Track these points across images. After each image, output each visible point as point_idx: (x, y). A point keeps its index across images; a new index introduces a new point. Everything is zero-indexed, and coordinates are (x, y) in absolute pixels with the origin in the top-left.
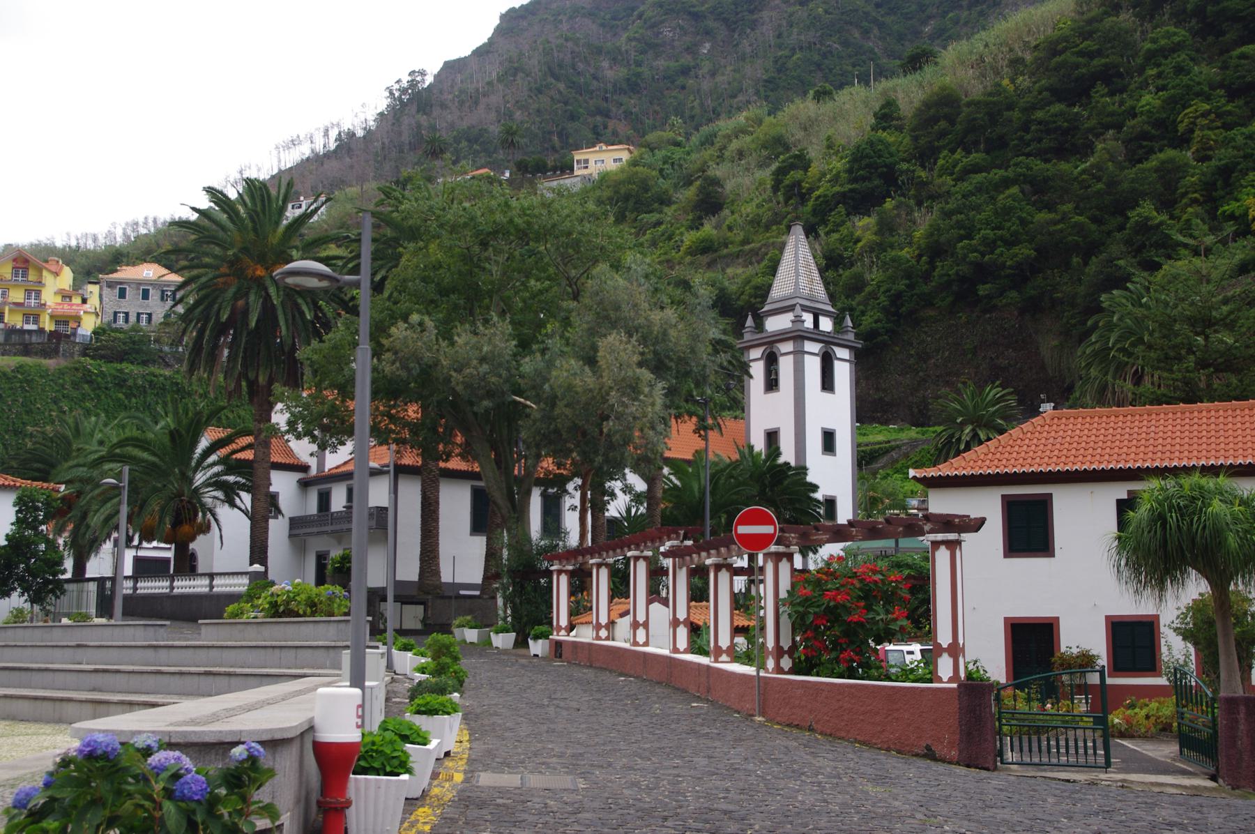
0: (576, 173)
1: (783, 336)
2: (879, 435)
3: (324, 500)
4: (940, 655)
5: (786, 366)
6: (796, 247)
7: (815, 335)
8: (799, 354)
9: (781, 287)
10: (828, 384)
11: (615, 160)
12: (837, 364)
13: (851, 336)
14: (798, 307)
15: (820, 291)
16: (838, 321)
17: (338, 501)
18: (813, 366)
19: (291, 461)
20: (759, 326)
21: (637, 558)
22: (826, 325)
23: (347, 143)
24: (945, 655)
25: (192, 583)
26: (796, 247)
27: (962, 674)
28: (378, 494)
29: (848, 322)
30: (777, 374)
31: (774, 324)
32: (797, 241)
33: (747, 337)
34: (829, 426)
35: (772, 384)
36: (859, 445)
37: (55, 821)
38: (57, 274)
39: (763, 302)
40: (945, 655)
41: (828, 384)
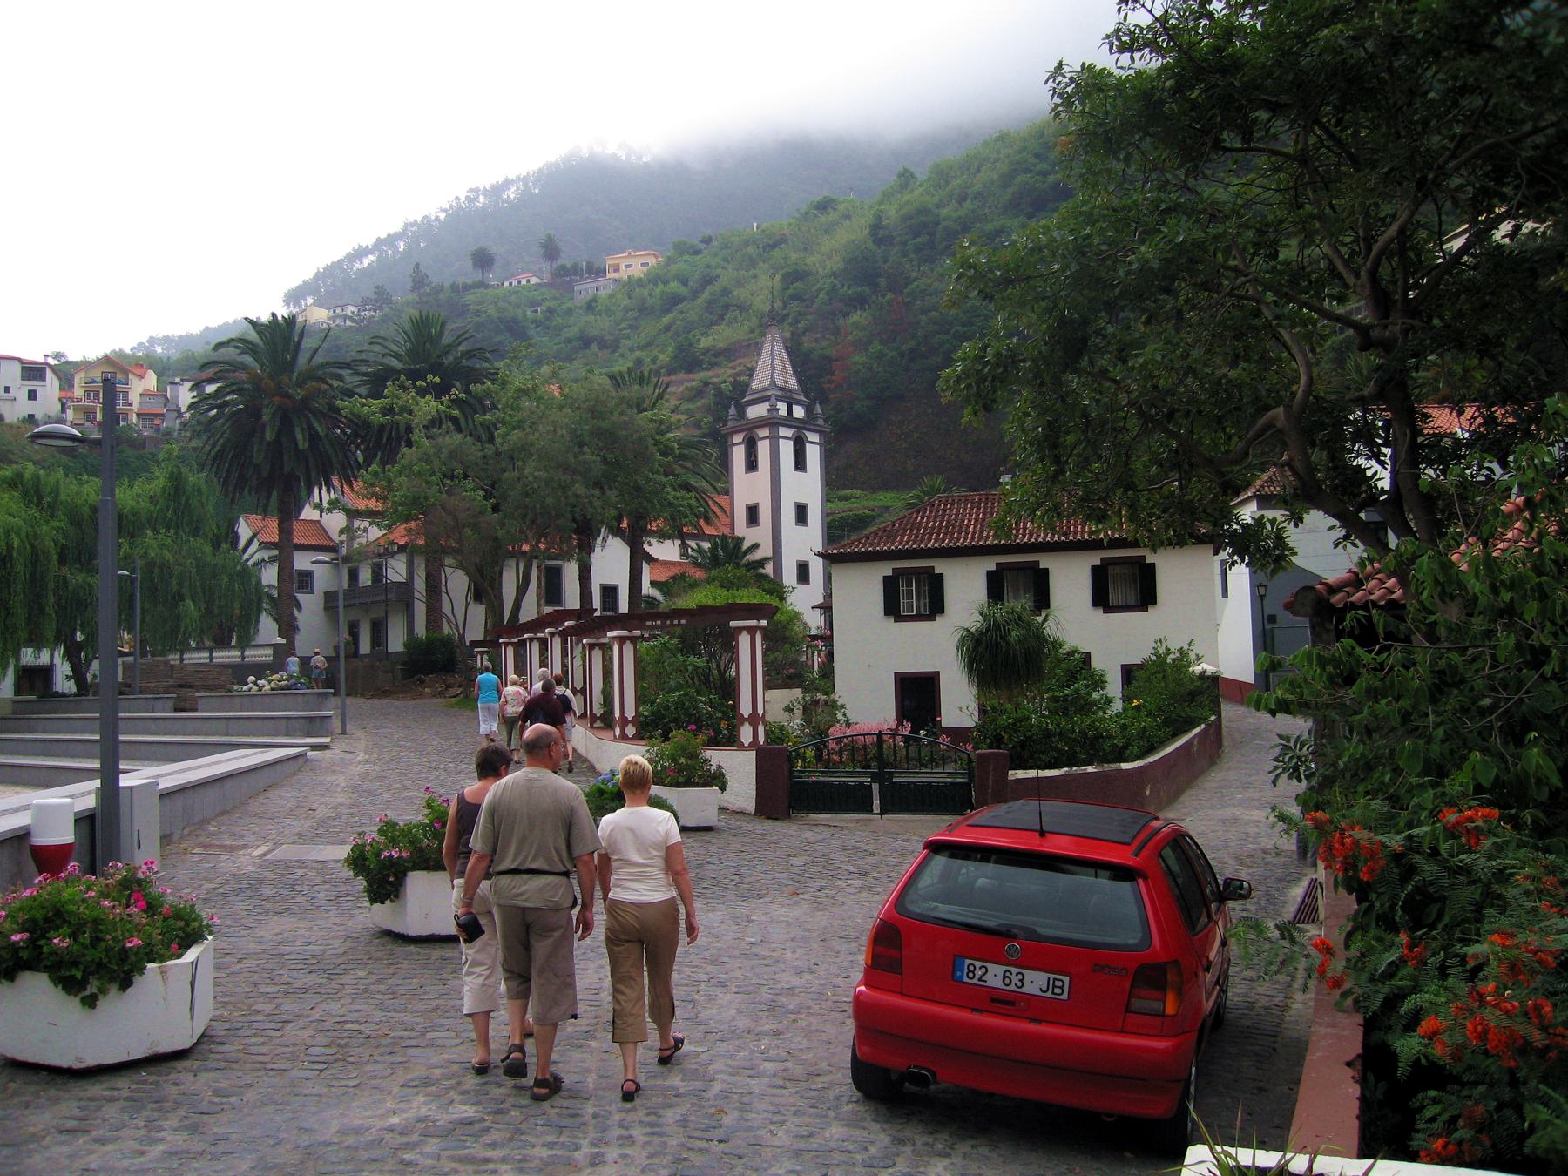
0: (608, 276)
1: (761, 423)
2: (861, 502)
3: (353, 575)
4: (742, 724)
5: (763, 448)
6: (773, 346)
7: (789, 421)
8: (774, 439)
9: (760, 381)
10: (800, 464)
11: (643, 265)
12: (808, 446)
13: (820, 422)
14: (773, 398)
15: (793, 383)
16: (809, 410)
17: (365, 577)
18: (787, 449)
19: (328, 543)
20: (741, 413)
21: (531, 640)
22: (799, 412)
23: (305, 283)
24: (747, 724)
25: (227, 654)
26: (773, 346)
27: (762, 739)
28: (397, 570)
29: (818, 409)
30: (756, 457)
31: (756, 412)
32: (773, 337)
33: (730, 424)
34: (802, 500)
35: (752, 465)
36: (828, 515)
37: (707, 761)
38: (141, 377)
39: (743, 393)
40: (747, 724)
41: (800, 464)
